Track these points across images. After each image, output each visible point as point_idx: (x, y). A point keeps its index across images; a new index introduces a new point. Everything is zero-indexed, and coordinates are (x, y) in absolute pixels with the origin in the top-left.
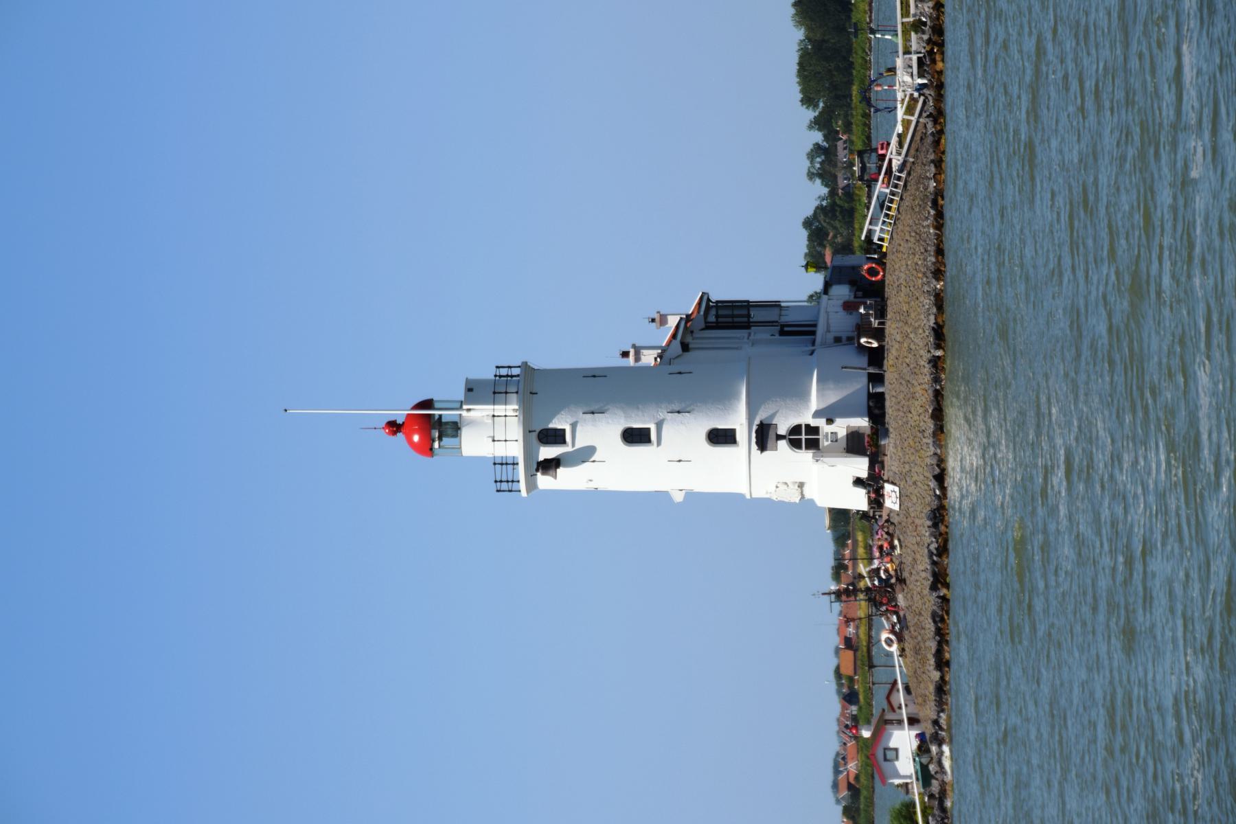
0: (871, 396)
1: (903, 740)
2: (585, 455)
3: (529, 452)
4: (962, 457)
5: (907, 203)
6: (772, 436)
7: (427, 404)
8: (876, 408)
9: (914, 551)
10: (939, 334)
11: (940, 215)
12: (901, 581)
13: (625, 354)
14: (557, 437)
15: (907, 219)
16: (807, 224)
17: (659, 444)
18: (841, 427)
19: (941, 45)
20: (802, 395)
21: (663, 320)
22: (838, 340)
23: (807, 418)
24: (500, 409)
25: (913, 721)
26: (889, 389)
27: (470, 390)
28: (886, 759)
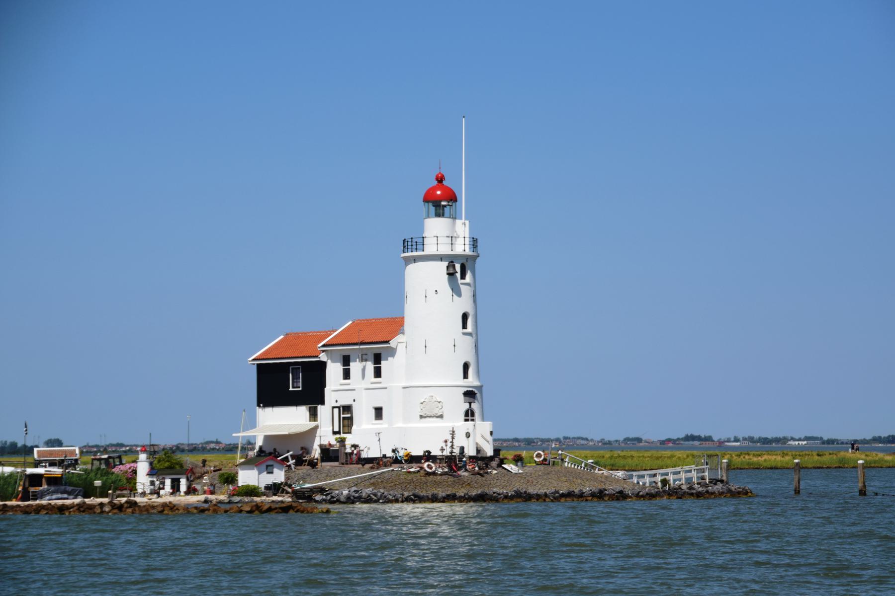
14: (463, 276)
17: (464, 334)
28: (267, 466)
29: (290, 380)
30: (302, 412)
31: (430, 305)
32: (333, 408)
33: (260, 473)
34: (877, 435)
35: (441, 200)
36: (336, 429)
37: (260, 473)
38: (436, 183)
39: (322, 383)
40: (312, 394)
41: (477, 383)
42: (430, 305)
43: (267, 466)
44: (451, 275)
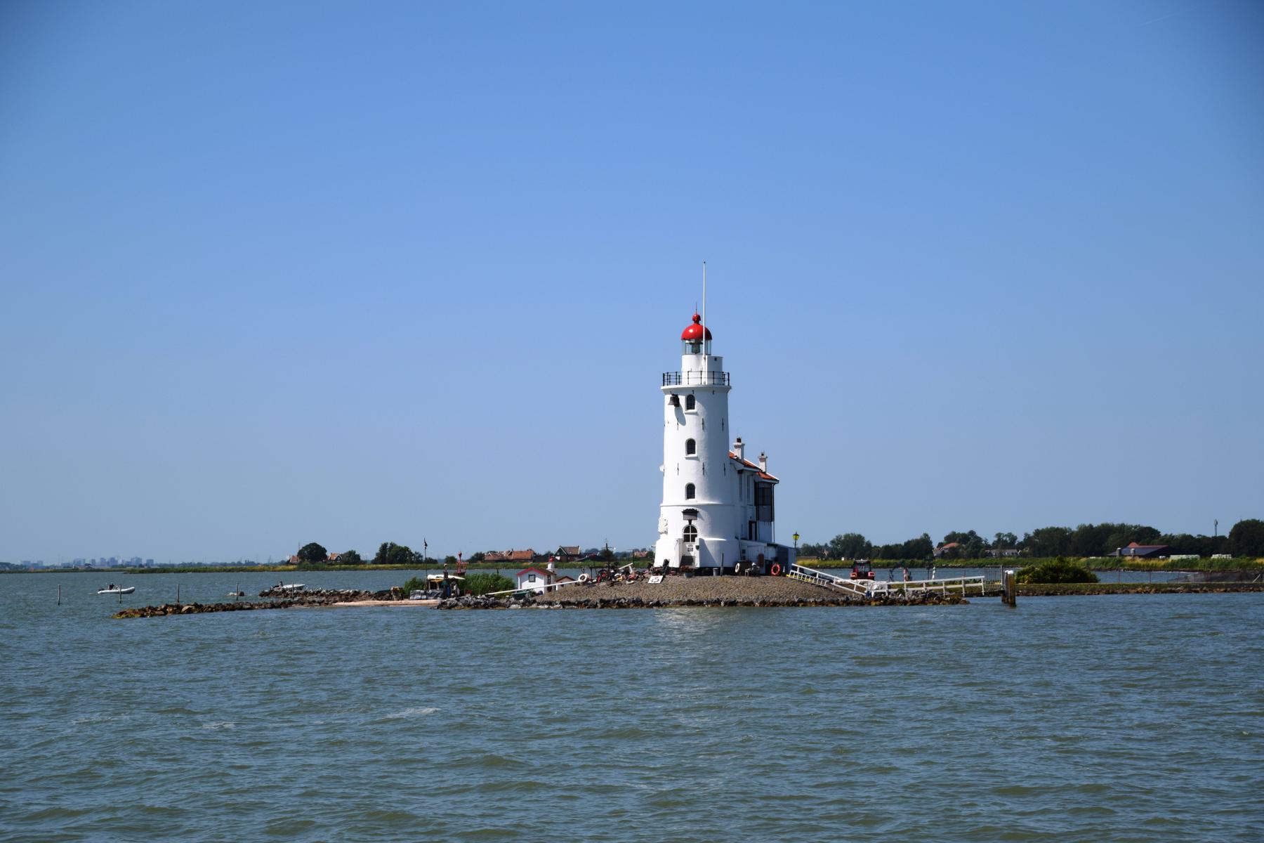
0: (711, 569)
1: (539, 585)
2: (681, 420)
3: (682, 390)
4: (673, 618)
5: (810, 587)
7: (709, 336)
8: (705, 571)
9: (626, 591)
10: (732, 604)
11: (794, 604)
12: (612, 585)
13: (739, 440)
14: (690, 405)
15: (801, 587)
16: (972, 533)
18: (695, 554)
19: (884, 604)
20: (713, 533)
21: (763, 460)
22: (744, 551)
23: (700, 535)
24: (705, 375)
25: (549, 589)
26: (715, 578)
27: (716, 359)
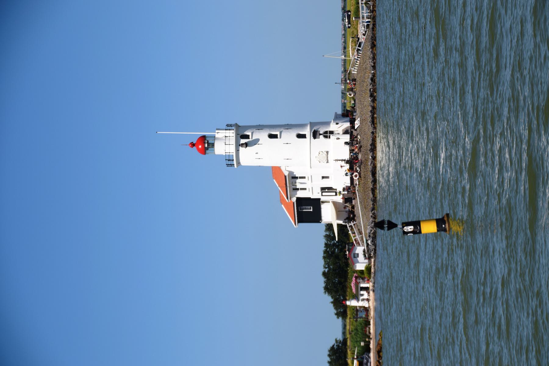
6: (318, 134)
14: (247, 137)
17: (280, 138)
28: (354, 257)
29: (308, 211)
30: (323, 206)
31: (264, 153)
32: (322, 195)
33: (358, 262)
34: (321, 281)
35: (204, 144)
36: (334, 194)
37: (358, 262)
38: (195, 147)
39: (309, 199)
40: (316, 203)
41: (308, 128)
42: (264, 153)
43: (354, 257)
44: (246, 145)
